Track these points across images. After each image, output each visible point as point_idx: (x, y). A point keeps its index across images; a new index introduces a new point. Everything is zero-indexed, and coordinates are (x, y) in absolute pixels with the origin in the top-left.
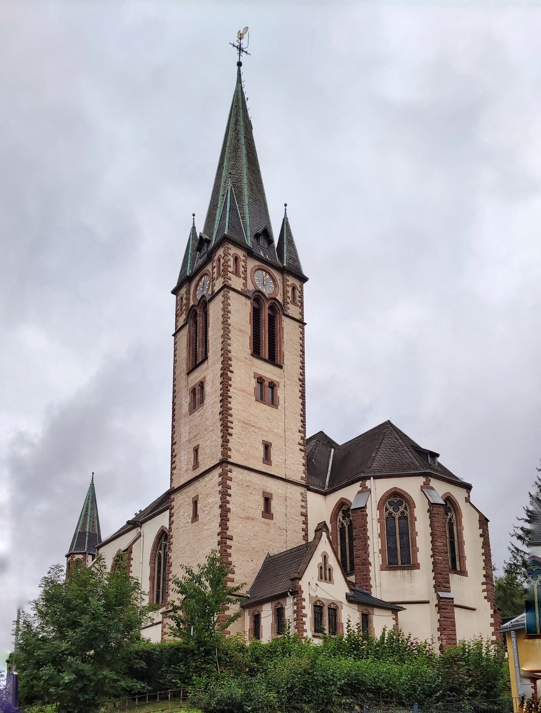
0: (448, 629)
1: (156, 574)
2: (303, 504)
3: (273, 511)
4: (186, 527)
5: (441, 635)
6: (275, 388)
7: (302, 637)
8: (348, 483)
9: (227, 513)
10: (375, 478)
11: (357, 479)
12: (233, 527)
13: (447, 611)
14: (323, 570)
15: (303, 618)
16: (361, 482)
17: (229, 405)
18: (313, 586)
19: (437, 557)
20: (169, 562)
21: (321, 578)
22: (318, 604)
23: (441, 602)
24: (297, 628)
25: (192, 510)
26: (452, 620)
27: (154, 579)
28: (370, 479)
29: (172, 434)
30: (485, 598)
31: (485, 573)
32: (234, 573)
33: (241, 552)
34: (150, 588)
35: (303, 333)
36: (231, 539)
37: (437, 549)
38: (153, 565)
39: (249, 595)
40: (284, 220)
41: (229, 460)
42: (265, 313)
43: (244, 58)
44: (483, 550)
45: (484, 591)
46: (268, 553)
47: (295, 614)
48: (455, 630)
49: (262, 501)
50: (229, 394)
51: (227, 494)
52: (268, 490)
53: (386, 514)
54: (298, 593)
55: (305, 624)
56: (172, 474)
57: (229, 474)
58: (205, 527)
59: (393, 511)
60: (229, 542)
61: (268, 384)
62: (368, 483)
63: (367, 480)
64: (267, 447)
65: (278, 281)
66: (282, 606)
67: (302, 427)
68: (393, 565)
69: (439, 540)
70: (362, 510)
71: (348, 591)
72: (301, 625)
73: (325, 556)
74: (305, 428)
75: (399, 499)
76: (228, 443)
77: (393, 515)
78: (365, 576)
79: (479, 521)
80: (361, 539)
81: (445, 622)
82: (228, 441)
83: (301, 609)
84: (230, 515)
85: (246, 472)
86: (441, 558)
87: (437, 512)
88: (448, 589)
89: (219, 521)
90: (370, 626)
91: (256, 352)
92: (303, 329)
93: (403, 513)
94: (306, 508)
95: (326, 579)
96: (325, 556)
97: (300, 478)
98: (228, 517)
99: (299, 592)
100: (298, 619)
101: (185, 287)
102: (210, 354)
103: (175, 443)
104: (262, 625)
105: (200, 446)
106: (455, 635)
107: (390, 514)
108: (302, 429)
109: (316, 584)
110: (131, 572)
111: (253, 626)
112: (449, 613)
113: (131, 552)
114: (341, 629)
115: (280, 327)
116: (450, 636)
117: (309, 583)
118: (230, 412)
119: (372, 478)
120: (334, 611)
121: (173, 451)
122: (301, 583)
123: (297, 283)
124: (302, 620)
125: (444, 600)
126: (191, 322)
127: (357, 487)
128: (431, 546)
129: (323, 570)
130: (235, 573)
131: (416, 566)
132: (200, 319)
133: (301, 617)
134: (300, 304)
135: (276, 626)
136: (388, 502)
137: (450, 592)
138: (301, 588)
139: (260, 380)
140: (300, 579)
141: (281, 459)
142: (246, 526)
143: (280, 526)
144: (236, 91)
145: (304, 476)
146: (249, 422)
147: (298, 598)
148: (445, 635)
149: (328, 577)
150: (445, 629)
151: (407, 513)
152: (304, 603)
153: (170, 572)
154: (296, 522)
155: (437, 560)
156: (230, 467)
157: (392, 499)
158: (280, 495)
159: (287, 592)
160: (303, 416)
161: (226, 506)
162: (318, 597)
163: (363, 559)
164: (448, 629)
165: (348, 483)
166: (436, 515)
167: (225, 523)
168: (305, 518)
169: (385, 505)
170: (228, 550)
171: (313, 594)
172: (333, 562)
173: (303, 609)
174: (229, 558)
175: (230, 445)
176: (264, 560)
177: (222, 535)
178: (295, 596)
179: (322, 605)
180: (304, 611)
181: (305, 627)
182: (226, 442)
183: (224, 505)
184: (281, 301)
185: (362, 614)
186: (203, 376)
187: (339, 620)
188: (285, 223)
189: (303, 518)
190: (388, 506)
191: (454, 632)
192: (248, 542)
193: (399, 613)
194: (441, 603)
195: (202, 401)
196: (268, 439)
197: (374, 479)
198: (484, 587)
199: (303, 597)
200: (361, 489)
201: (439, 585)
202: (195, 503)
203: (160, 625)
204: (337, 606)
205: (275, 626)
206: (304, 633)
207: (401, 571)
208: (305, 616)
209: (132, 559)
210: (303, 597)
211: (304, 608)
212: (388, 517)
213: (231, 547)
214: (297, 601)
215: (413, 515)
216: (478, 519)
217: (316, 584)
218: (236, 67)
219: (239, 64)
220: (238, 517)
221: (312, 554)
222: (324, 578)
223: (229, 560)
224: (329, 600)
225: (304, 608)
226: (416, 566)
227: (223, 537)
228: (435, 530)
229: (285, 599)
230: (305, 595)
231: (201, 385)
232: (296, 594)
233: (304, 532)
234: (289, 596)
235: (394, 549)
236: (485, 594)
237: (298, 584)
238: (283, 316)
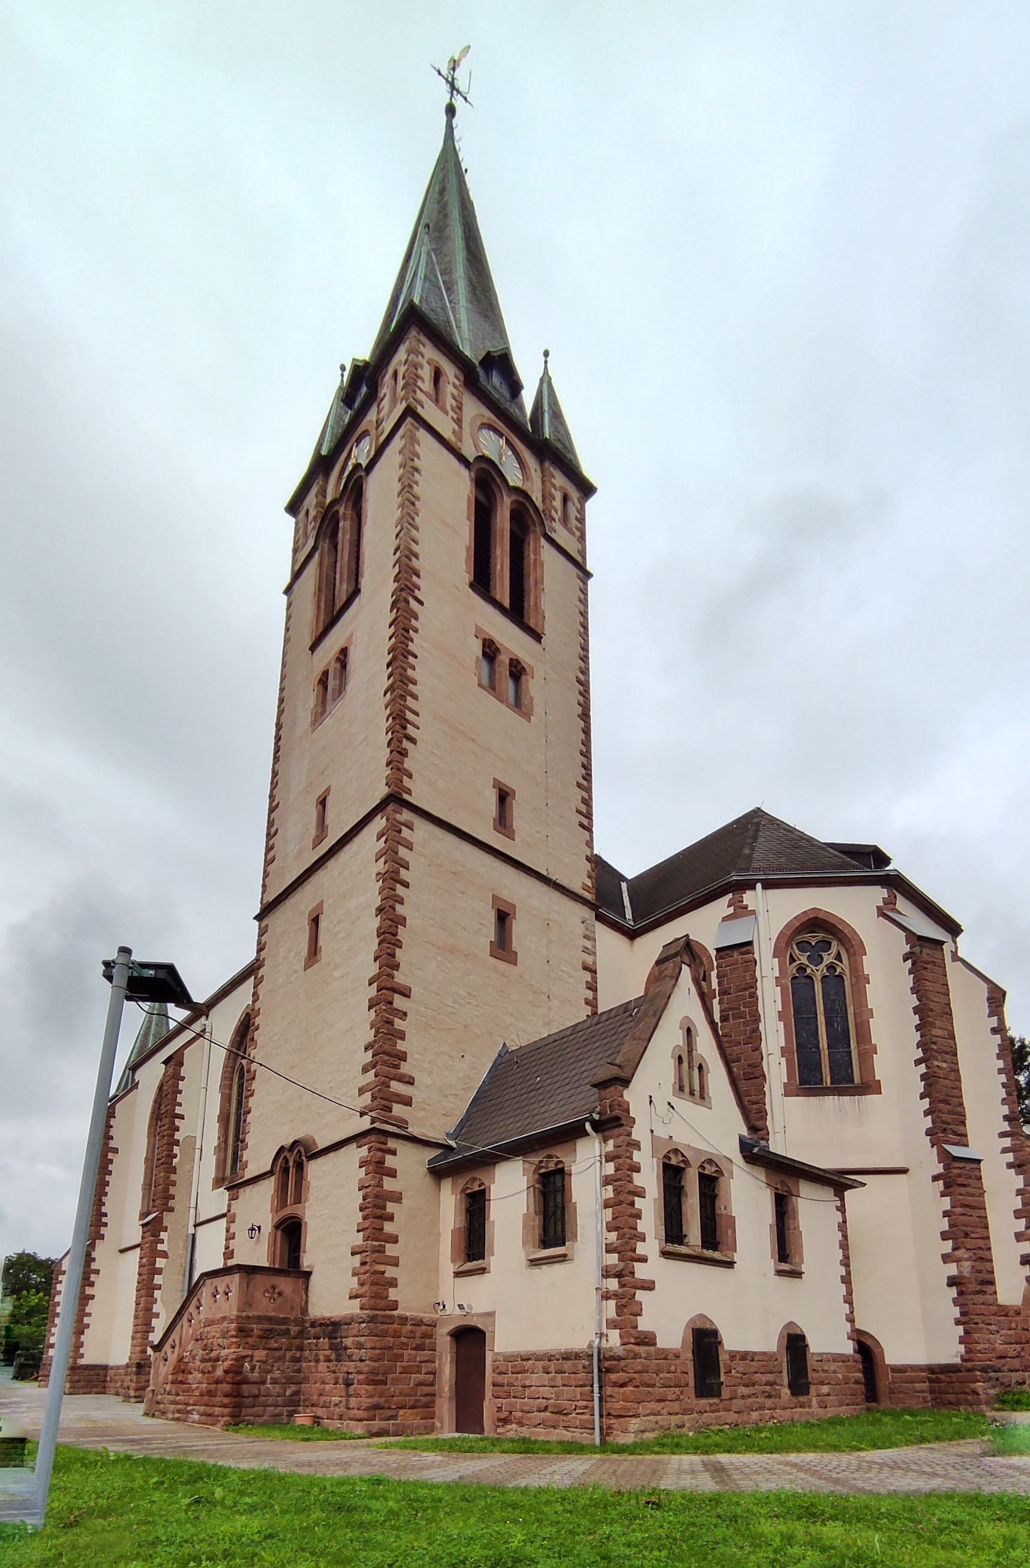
0: (973, 1235)
1: (233, 1110)
2: (589, 944)
3: (515, 946)
4: (291, 982)
5: (954, 1249)
6: (523, 677)
7: (634, 1255)
8: (698, 900)
9: (397, 927)
10: (768, 885)
11: (719, 890)
12: (411, 965)
13: (969, 1190)
14: (685, 1065)
15: (636, 1198)
16: (730, 896)
17: (410, 672)
18: (661, 1107)
19: (936, 1063)
20: (249, 1071)
21: (681, 1089)
22: (674, 1162)
23: (955, 1168)
24: (616, 1229)
25: (307, 939)
26: (981, 1213)
27: (228, 1121)
28: (754, 888)
29: (272, 790)
30: (1010, 1166)
31: (1007, 1112)
32: (412, 1084)
33: (433, 1032)
34: (219, 1138)
35: (584, 591)
36: (406, 993)
37: (935, 1043)
38: (228, 1091)
39: (453, 1143)
40: (542, 380)
41: (406, 796)
42: (502, 521)
43: (458, 102)
44: (1001, 1061)
45: (1005, 1150)
46: (505, 1044)
47: (610, 1188)
48: (988, 1238)
49: (491, 918)
50: (411, 647)
51: (397, 878)
52: (505, 895)
53: (792, 969)
54: (622, 1125)
55: (640, 1217)
56: (266, 874)
57: (406, 832)
58: (336, 974)
59: (808, 963)
60: (399, 1002)
61: (507, 661)
62: (749, 898)
63: (747, 892)
64: (504, 796)
65: (533, 471)
66: (560, 1166)
67: (584, 779)
68: (810, 1084)
69: (938, 1023)
70: (745, 949)
71: (745, 1132)
72: (631, 1220)
73: (689, 1030)
74: (589, 781)
75: (821, 935)
76: (406, 759)
77: (809, 971)
78: (754, 1107)
79: (988, 999)
80: (741, 1017)
81: (966, 1217)
82: (403, 753)
83: (629, 1173)
84: (402, 933)
85: (451, 838)
86: (944, 1065)
87: (931, 959)
88: (962, 1139)
89: (374, 946)
90: (792, 1227)
91: (482, 582)
92: (585, 584)
93: (831, 967)
94: (594, 953)
95: (692, 1093)
96: (689, 1030)
97: (580, 884)
98: (398, 937)
99: (622, 1122)
100: (621, 1203)
101: (315, 485)
102: (365, 582)
103: (277, 806)
104: (491, 1219)
105: (332, 789)
106: (989, 1249)
107: (802, 969)
108: (585, 783)
109: (669, 1104)
110: (180, 1105)
111: (463, 1224)
112: (973, 1195)
113: (182, 1064)
114: (730, 1232)
115: (535, 560)
116: (981, 1253)
117: (651, 1097)
118: (411, 687)
119: (759, 886)
120: (710, 1184)
121: (271, 823)
122: (628, 1095)
123: (574, 494)
124: (632, 1204)
125: (961, 1165)
126: (325, 545)
127: (721, 907)
128: (917, 1037)
129: (685, 1065)
130: (416, 1083)
131: (870, 1087)
132: (345, 526)
133: (630, 1197)
134: (578, 534)
135: (537, 1222)
136: (797, 944)
137: (967, 1145)
138: (628, 1111)
139: (490, 651)
140: (626, 1082)
141: (538, 832)
142: (448, 968)
143: (533, 982)
144: (444, 150)
145: (589, 883)
146: (460, 727)
147: (621, 1138)
148: (968, 1249)
149: (697, 1088)
150: (966, 1235)
151: (844, 967)
152: (637, 1156)
153: (250, 1093)
154: (571, 981)
155: (936, 1070)
156: (406, 815)
157: (807, 936)
158: (535, 913)
159: (586, 1119)
160: (585, 756)
161: (394, 909)
162: (674, 1139)
163: (749, 1066)
164: (973, 1235)
165: (698, 900)
166: (927, 966)
167: (389, 951)
168: (592, 977)
169: (790, 949)
170: (397, 1021)
171: (662, 1133)
172: (706, 1046)
173: (634, 1174)
174: (399, 1041)
175: (408, 764)
176: (493, 1059)
177: (382, 981)
178: (606, 1133)
179: (682, 1165)
180: (638, 1179)
181: (642, 1226)
182: (400, 753)
183: (390, 904)
184: (539, 504)
185: (776, 1194)
186: (347, 635)
187: (725, 1208)
188: (546, 381)
189: (588, 976)
190: (797, 951)
191: (986, 1241)
192: (453, 1010)
193: (848, 1194)
194: (954, 1171)
195: (341, 690)
196: (510, 782)
197: (764, 888)
198: (1007, 1142)
199: (633, 1137)
200: (731, 910)
201: (945, 1129)
202: (315, 921)
203: (224, 1220)
204: (720, 1172)
205: (537, 1223)
206: (638, 1243)
207: (836, 1097)
208: (640, 1193)
209: (180, 1092)
210: (633, 1137)
211: (637, 1170)
212: (796, 977)
213: (405, 1014)
214: (615, 1147)
215: (860, 969)
216: (986, 995)
217: (669, 1104)
218: (443, 118)
219: (451, 111)
220: (426, 942)
221: (658, 1016)
222: (687, 1089)
223: (398, 1047)
224: (699, 1152)
225: (637, 1170)
226: (870, 1087)
227: (383, 985)
228: (928, 998)
229: (569, 1145)
230: (639, 1133)
231: (342, 658)
232: (616, 1127)
233: (589, 1008)
234: (588, 1134)
235: (811, 1049)
236: (1010, 1157)
237: (622, 1096)
238: (542, 540)
